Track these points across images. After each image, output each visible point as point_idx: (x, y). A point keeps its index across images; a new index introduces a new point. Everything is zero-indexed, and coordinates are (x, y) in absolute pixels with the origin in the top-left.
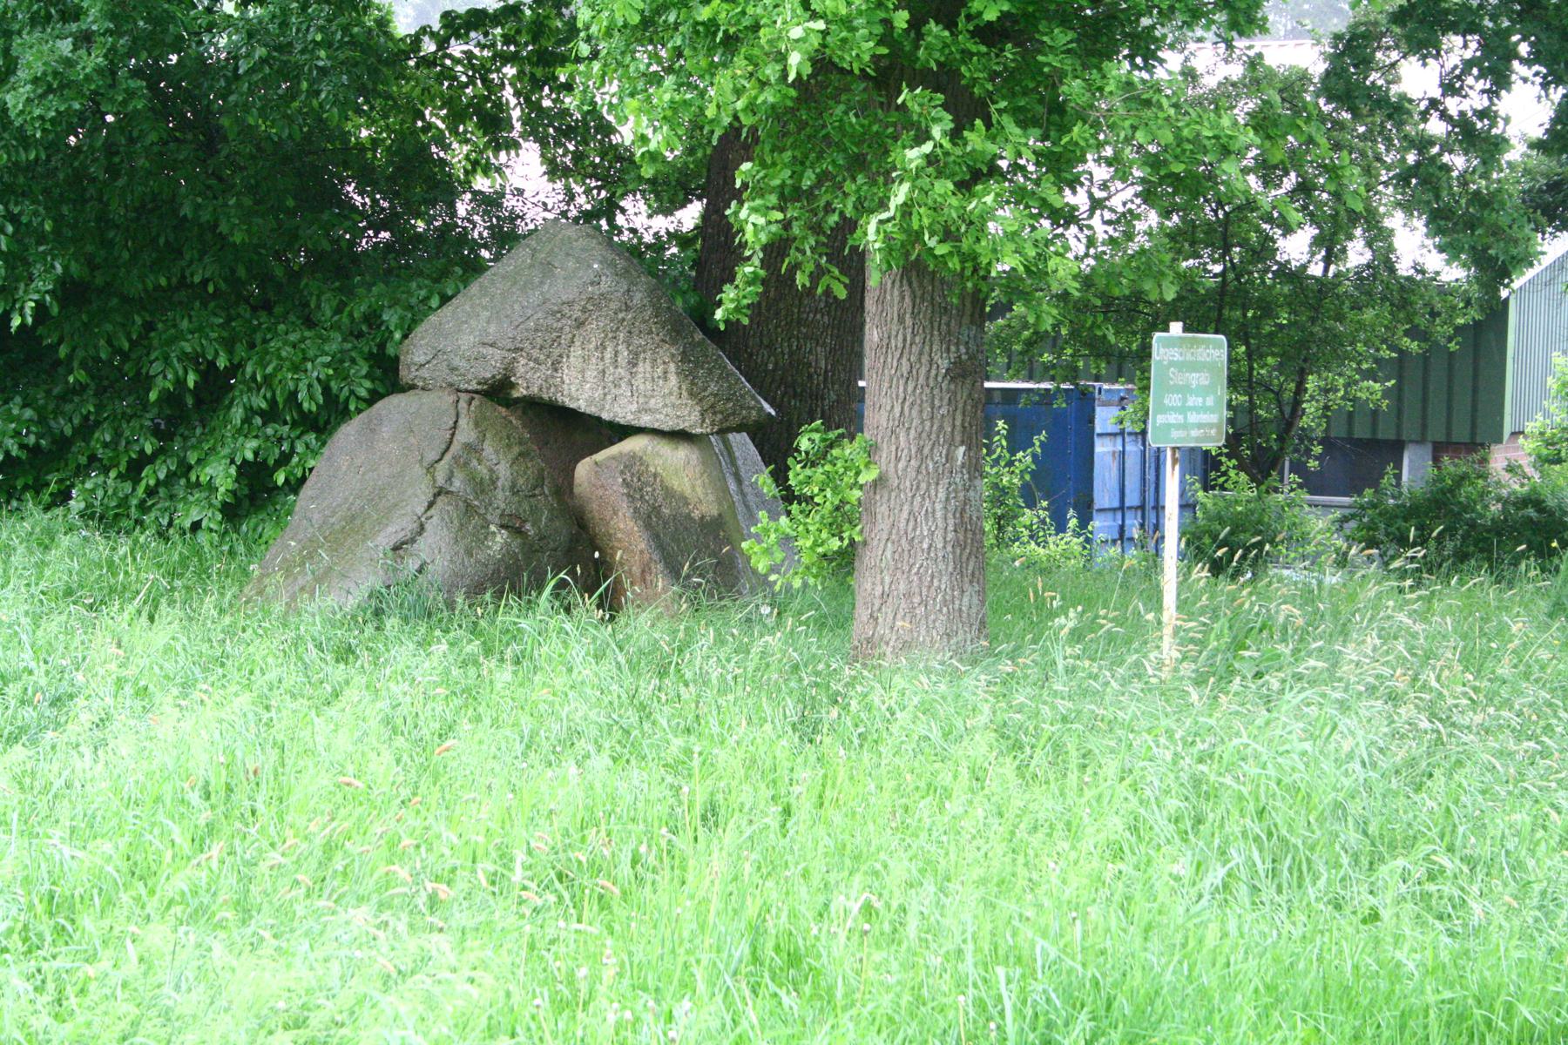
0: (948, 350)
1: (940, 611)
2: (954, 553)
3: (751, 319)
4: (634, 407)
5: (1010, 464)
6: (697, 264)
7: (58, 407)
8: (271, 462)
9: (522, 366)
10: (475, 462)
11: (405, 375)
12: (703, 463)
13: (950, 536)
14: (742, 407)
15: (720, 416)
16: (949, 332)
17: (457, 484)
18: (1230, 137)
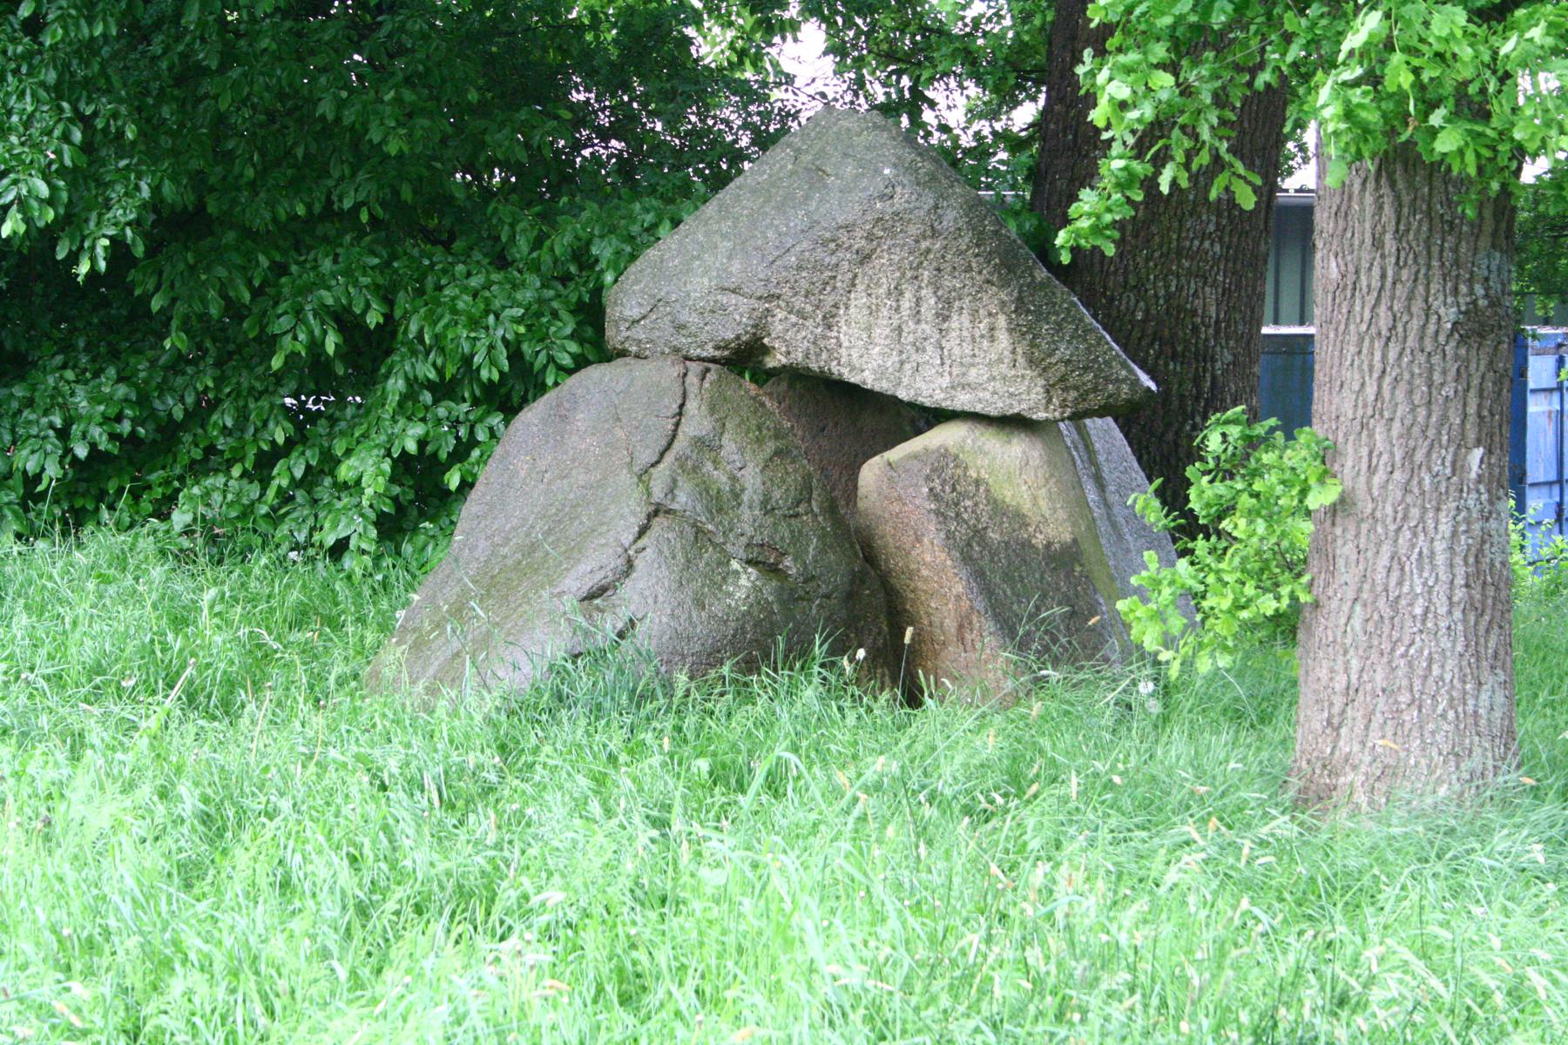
0: (1456, 291)
1: (1443, 716)
2: (1465, 621)
3: (1119, 244)
4: (945, 381)
6: (1035, 175)
7: (165, 380)
8: (443, 456)
9: (779, 322)
10: (709, 466)
11: (615, 335)
12: (1049, 463)
13: (1459, 594)
14: (1107, 380)
15: (1073, 394)
16: (1457, 263)
17: (683, 499)
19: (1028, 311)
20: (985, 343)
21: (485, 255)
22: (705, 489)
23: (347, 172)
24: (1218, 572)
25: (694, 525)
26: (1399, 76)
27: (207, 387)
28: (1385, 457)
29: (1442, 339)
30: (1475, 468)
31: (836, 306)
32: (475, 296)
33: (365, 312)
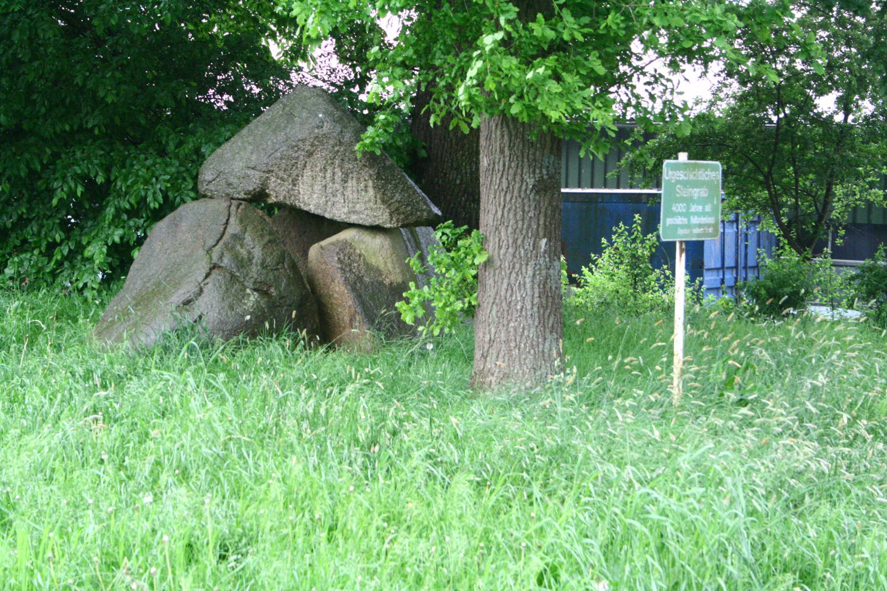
0: (534, 172)
2: (539, 312)
4: (346, 210)
5: (643, 242)
8: (132, 243)
9: (273, 182)
10: (238, 247)
11: (202, 188)
13: (536, 300)
14: (417, 210)
15: (402, 216)
16: (535, 160)
17: (226, 261)
18: (721, 22)
19: (382, 179)
20: (363, 193)
21: (155, 150)
22: (236, 257)
23: (90, 110)
24: (440, 292)
25: (230, 273)
26: (491, 85)
27: (23, 213)
28: (505, 242)
29: (528, 192)
30: (543, 247)
31: (297, 176)
32: (148, 169)
33: (95, 177)
